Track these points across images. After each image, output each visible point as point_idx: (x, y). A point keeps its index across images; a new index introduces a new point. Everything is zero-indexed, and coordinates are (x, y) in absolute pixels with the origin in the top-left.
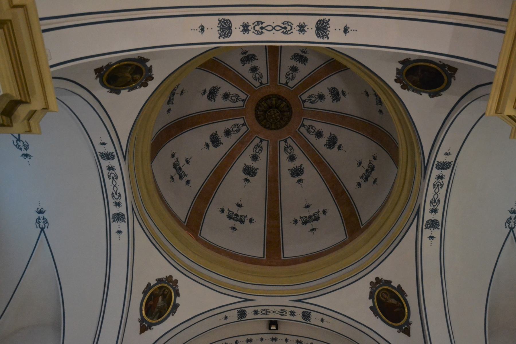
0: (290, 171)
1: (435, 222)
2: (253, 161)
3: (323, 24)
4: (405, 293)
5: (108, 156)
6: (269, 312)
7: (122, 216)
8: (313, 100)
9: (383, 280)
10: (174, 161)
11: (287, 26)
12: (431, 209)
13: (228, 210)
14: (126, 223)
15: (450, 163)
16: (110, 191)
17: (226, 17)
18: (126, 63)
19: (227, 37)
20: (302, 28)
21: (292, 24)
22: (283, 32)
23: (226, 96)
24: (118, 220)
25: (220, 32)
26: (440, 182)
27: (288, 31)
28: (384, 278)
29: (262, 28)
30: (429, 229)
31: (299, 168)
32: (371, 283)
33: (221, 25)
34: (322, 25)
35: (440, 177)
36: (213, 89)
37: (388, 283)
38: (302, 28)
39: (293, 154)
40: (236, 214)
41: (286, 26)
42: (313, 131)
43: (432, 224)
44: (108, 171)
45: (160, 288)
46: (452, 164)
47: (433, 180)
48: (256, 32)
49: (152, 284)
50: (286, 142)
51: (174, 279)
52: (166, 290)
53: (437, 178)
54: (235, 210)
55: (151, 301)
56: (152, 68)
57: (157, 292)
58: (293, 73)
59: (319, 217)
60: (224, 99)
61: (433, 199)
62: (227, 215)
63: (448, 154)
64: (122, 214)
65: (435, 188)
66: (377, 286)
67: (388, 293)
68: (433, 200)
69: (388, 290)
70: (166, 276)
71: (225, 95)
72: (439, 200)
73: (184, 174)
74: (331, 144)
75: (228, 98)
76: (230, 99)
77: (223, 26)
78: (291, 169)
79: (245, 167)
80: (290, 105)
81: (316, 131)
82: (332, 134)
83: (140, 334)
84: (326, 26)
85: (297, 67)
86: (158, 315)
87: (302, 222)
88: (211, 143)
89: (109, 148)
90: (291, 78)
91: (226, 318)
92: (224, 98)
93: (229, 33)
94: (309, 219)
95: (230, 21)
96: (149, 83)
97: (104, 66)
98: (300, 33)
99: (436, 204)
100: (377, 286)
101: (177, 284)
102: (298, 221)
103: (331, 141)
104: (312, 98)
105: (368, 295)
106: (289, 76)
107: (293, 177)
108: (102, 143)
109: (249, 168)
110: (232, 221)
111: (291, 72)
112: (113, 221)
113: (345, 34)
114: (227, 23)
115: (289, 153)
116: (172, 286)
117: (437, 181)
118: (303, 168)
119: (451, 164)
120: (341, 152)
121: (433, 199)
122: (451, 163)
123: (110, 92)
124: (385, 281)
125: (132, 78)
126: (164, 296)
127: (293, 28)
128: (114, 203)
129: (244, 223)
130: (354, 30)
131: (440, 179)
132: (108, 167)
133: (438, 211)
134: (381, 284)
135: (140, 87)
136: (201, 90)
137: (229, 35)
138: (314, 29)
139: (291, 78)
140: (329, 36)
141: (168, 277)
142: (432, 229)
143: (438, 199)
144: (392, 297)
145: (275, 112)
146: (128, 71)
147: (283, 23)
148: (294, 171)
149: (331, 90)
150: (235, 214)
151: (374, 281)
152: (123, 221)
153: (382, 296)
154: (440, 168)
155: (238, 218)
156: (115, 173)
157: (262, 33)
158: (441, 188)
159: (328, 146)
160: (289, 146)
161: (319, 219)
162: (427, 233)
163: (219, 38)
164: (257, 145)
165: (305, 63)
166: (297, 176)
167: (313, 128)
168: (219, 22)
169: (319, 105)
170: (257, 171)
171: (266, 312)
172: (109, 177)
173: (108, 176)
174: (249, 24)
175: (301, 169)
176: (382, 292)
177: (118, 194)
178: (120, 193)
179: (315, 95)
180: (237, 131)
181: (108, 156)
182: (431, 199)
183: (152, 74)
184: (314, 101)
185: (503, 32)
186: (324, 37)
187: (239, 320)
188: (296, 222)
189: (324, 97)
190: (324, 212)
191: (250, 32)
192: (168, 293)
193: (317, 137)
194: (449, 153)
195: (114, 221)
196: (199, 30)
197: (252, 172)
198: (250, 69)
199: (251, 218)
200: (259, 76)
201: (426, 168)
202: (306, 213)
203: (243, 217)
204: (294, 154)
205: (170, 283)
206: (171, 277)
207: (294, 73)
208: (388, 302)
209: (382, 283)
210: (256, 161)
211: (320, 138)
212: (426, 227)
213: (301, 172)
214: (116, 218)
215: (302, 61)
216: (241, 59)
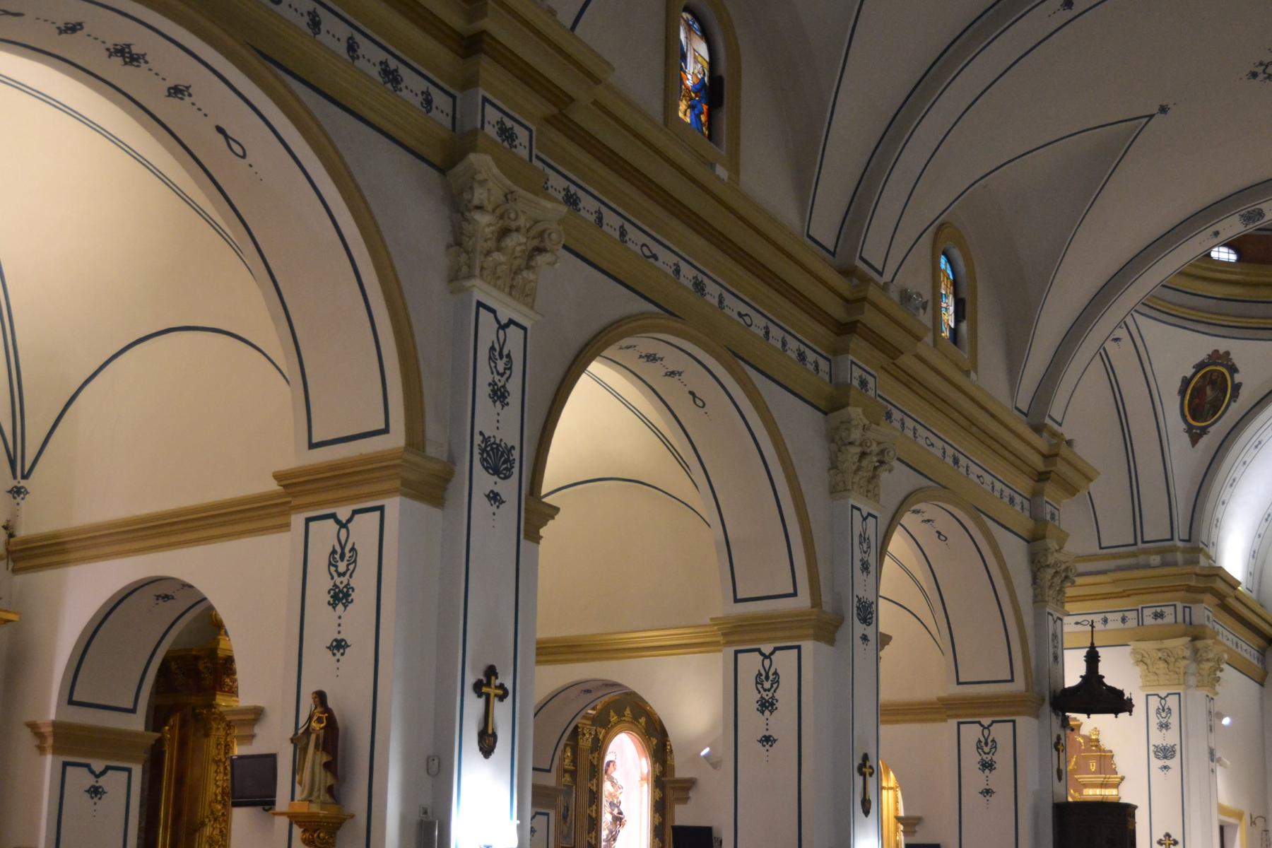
6: (343, 548)
11: (348, 561)
15: (1173, 747)
41: (347, 558)
51: (1221, 352)
52: (1214, 374)
57: (1200, 384)
83: (1193, 446)
86: (1211, 412)
116: (1221, 365)
126: (1213, 383)
137: (485, 464)
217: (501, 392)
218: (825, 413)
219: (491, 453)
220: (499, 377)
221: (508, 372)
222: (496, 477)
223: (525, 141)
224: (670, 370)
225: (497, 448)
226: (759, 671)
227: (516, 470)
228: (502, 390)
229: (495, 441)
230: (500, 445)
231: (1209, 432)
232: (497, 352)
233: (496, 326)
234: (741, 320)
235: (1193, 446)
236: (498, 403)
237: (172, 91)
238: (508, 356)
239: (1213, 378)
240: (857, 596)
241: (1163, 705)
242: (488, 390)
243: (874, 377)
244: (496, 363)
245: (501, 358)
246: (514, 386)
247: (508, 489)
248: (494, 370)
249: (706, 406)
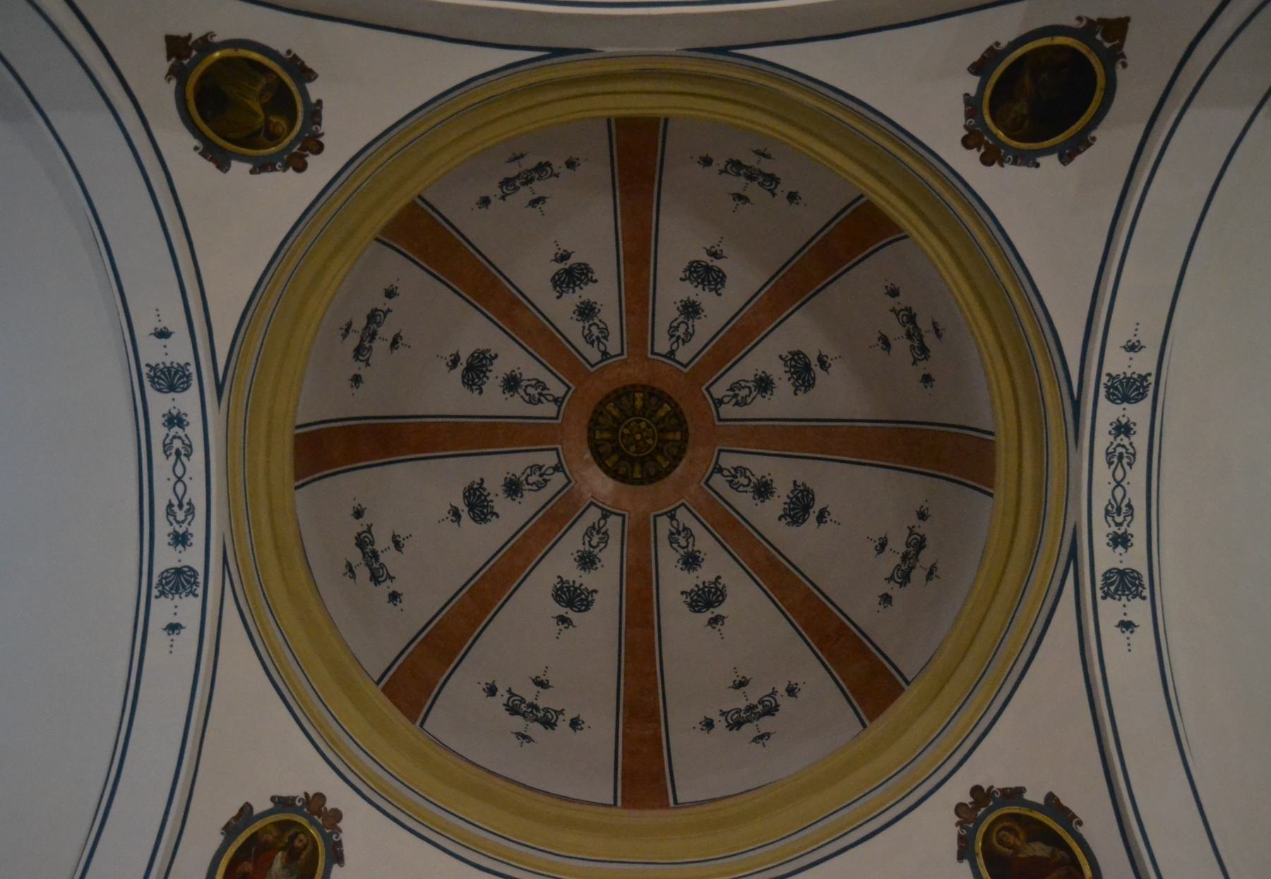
0: (687, 598)
1: (1130, 577)
2: (581, 569)
4: (1074, 816)
5: (171, 379)
7: (191, 576)
8: (742, 397)
9: (995, 792)
10: (360, 530)
12: (1111, 536)
13: (507, 691)
14: (199, 600)
16: (163, 495)
18: (255, 56)
23: (512, 383)
24: (176, 589)
26: (1123, 446)
28: (999, 784)
30: (1114, 599)
31: (713, 586)
32: (960, 808)
35: (1123, 429)
36: (478, 357)
37: (1014, 795)
39: (693, 550)
40: (532, 703)
42: (745, 482)
43: (1122, 580)
44: (165, 430)
45: (283, 826)
46: (1150, 384)
47: (1104, 439)
49: (257, 810)
50: (672, 517)
51: (329, 805)
52: (302, 836)
53: (1113, 432)
54: (529, 693)
55: (246, 863)
56: (321, 107)
57: (270, 838)
58: (688, 320)
59: (777, 706)
60: (506, 392)
61: (1113, 502)
62: (506, 703)
63: (1137, 347)
64: (191, 569)
65: (1113, 467)
66: (979, 813)
67: (1017, 828)
68: (1113, 507)
69: (1015, 817)
70: (306, 794)
71: (508, 379)
72: (1129, 506)
73: (385, 571)
74: (797, 513)
75: (516, 389)
76: (523, 394)
78: (689, 591)
79: (558, 586)
80: (681, 412)
81: (756, 481)
82: (798, 484)
83: (1127, 20)
85: (697, 303)
87: (726, 724)
88: (466, 509)
89: (178, 351)
90: (682, 336)
92: (506, 388)
94: (748, 714)
96: (311, 159)
97: (195, 37)
99: (1125, 520)
100: (979, 813)
101: (339, 825)
102: (715, 723)
103: (798, 503)
104: (740, 390)
105: (954, 847)
106: (678, 331)
107: (696, 612)
108: (159, 329)
109: (572, 589)
110: (519, 719)
111: (681, 319)
112: (160, 596)
115: (683, 548)
116: (320, 829)
117: (1115, 444)
118: (724, 587)
119: (1147, 381)
120: (827, 528)
121: (1113, 502)
122: (1148, 378)
123: (201, 154)
124: (1003, 791)
125: (267, 122)
126: (293, 856)
128: (169, 535)
129: (556, 728)
131: (1122, 436)
132: (166, 418)
133: (1133, 540)
134: (991, 803)
135: (285, 168)
136: (448, 352)
137: (1136, 575)
139: (682, 336)
141: (311, 795)
142: (1124, 598)
143: (1126, 501)
144: (1031, 838)
145: (643, 425)
146: (259, 88)
148: (699, 596)
149: (789, 362)
150: (527, 702)
151: (968, 799)
152: (191, 592)
153: (1000, 841)
154: (1119, 399)
155: (538, 714)
156: (186, 436)
158: (1130, 465)
159: (789, 520)
160: (681, 529)
161: (778, 710)
162: (1111, 611)
164: (593, 527)
165: (719, 289)
166: (708, 609)
167: (745, 473)
169: (761, 407)
170: (594, 598)
172: (165, 452)
173: (164, 445)
175: (717, 589)
176: (997, 829)
177: (186, 507)
178: (193, 502)
179: (748, 382)
180: (540, 486)
181: (171, 379)
182: (1107, 503)
183: (320, 132)
184: (744, 398)
188: (709, 724)
189: (772, 382)
190: (791, 691)
192: (305, 847)
193: (759, 498)
194: (1137, 344)
195: (162, 593)
197: (579, 598)
198: (575, 308)
199: (575, 716)
200: (593, 536)
201: (1077, 405)
202: (739, 701)
203: (553, 713)
204: (696, 549)
205: (316, 817)
206: (320, 797)
207: (691, 320)
208: (1021, 856)
209: (995, 799)
210: (592, 570)
211: (768, 498)
212: (1104, 592)
213: (719, 596)
214: (170, 586)
215: (710, 284)
216: (554, 277)
222: (1121, 568)
226: (170, 501)
230: (173, 367)
231: (1080, 19)
235: (1127, 20)
239: (297, 844)
241: (601, 525)
244: (183, 443)
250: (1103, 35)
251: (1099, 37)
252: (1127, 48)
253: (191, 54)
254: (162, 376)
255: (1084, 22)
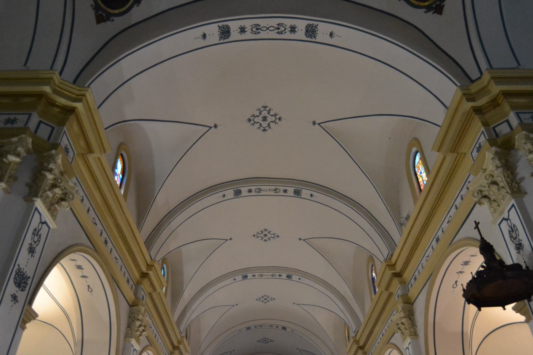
3: (225, 36)
17: (309, 39)
19: (311, 25)
20: (242, 30)
21: (251, 32)
22: (259, 26)
25: (316, 30)
27: (255, 27)
29: (278, 29)
33: (314, 34)
34: (225, 35)
38: (243, 30)
48: (284, 25)
77: (313, 34)
84: (222, 35)
91: (224, 196)
93: (308, 27)
95: (307, 37)
98: (244, 26)
113: (204, 33)
114: (309, 35)
127: (251, 29)
130: (198, 38)
138: (231, 31)
140: (218, 28)
147: (259, 33)
157: (278, 25)
163: (317, 25)
168: (316, 37)
171: (513, 232)
174: (289, 32)
185: (106, 129)
186: (222, 26)
187: (301, 189)
191: (289, 26)
196: (334, 35)
217: (33, 250)
218: (130, 307)
219: (20, 276)
220: (34, 243)
221: (38, 242)
223: (72, 157)
224: (84, 275)
225: (23, 275)
226: (276, 33)
227: (27, 289)
228: (34, 249)
229: (23, 271)
230: (220, 32)
232: (36, 233)
233: (39, 221)
234: (115, 260)
236: (30, 254)
237: (14, 296)
238: (40, 235)
240: (19, 265)
242: (28, 246)
243: (146, 296)
244: (34, 237)
245: (37, 236)
246: (38, 249)
247: (22, 296)
248: (33, 239)
249: (93, 290)
250: (102, 15)
251: (104, 15)
252: (93, 12)
253: (435, 6)
254: (312, 29)
255: (111, 19)
